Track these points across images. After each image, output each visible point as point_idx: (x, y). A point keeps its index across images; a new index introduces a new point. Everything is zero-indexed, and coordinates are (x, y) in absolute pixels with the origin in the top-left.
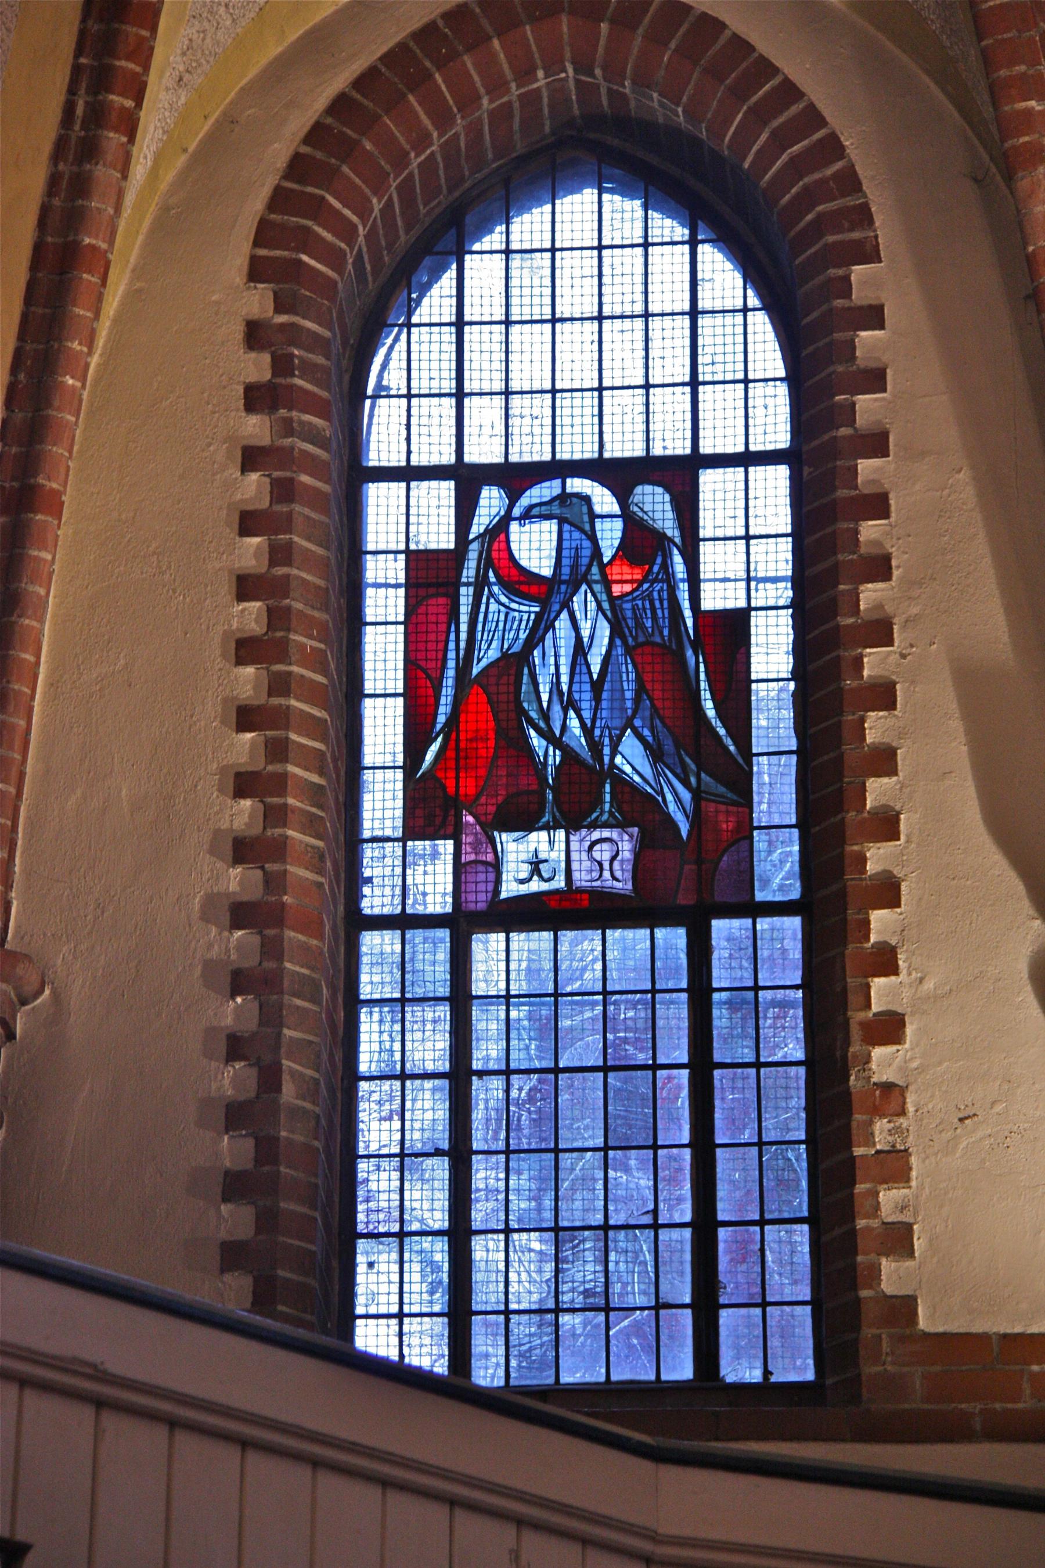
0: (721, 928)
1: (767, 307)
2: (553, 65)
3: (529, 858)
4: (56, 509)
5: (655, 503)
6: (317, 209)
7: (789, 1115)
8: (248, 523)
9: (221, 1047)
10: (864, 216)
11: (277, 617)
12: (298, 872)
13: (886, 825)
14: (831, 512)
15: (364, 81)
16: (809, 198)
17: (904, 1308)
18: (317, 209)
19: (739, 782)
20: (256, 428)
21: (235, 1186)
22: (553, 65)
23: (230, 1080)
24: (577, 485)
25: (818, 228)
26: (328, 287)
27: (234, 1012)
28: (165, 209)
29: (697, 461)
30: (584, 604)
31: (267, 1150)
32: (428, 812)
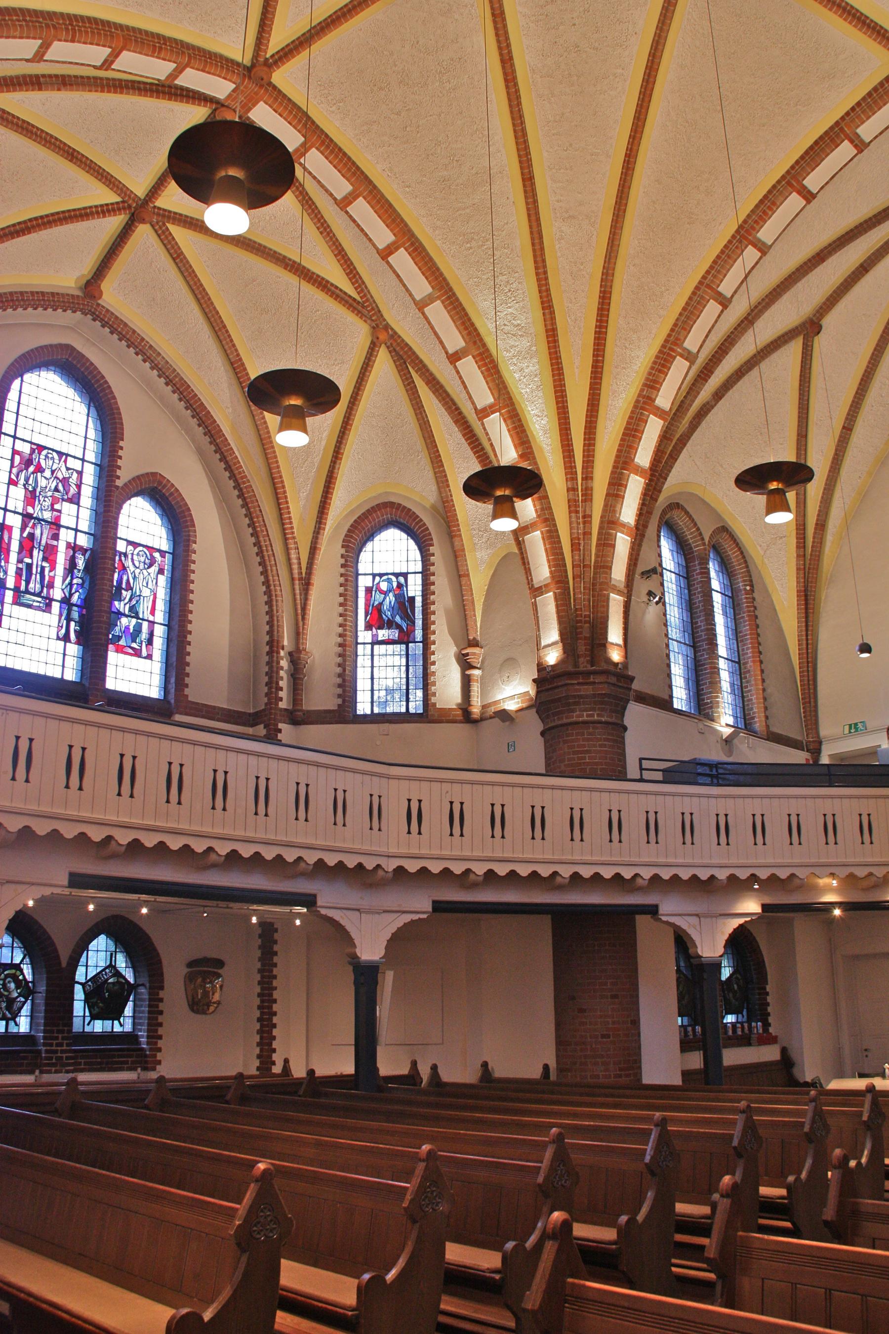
0: (410, 645)
2: (387, 514)
3: (383, 634)
4: (313, 585)
5: (402, 580)
6: (352, 537)
7: (420, 670)
8: (341, 585)
10: (432, 539)
11: (345, 600)
12: (348, 639)
13: (434, 643)
14: (426, 595)
16: (424, 536)
17: (435, 704)
18: (352, 537)
19: (414, 623)
21: (340, 686)
22: (387, 514)
24: (390, 576)
25: (425, 541)
26: (353, 549)
27: (339, 660)
29: (408, 573)
30: (391, 595)
31: (344, 680)
32: (368, 627)
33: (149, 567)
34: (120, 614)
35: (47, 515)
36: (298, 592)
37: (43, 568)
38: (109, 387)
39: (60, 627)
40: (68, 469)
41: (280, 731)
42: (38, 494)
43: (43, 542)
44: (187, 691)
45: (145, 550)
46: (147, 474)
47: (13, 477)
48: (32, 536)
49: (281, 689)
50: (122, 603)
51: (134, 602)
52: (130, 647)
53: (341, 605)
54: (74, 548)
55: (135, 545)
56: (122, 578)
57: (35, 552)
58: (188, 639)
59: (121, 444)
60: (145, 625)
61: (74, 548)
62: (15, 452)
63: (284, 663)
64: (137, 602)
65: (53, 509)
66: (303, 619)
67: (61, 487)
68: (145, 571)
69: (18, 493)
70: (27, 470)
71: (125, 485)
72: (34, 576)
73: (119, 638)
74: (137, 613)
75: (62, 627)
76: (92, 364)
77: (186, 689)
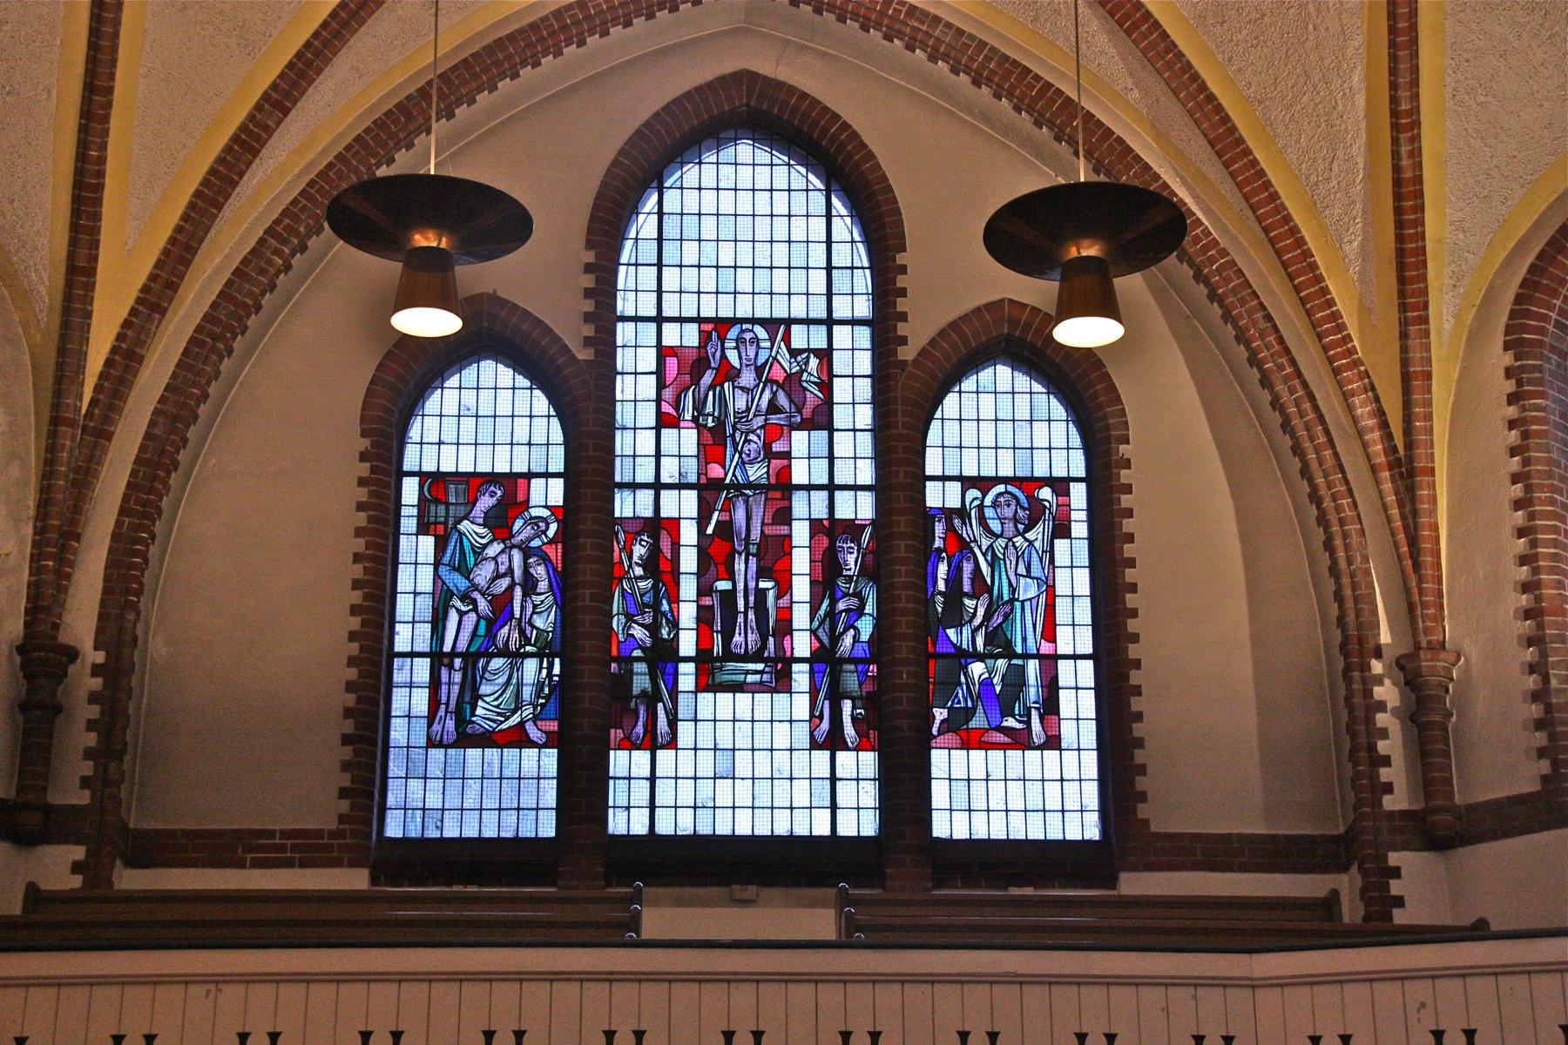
1: (559, 415)
8: (1513, 452)
9: (1527, 669)
11: (1528, 489)
15: (1540, 257)
17: (1146, 822)
18: (1527, 314)
20: (1512, 412)
21: (1539, 725)
23: (1532, 682)
27: (1530, 654)
28: (1471, 331)
33: (1028, 528)
34: (964, 657)
35: (756, 473)
36: (1391, 499)
37: (760, 594)
38: (855, 135)
39: (815, 717)
40: (794, 353)
41: (1396, 873)
42: (729, 430)
43: (756, 535)
44: (1143, 811)
45: (1010, 488)
46: (977, 310)
47: (666, 408)
48: (726, 528)
49: (1386, 761)
50: (966, 631)
51: (997, 620)
52: (999, 729)
53: (1518, 504)
54: (830, 531)
55: (983, 483)
56: (960, 569)
57: (739, 565)
58: (1133, 681)
59: (901, 259)
60: (1032, 667)
61: (830, 531)
62: (663, 352)
63: (1386, 692)
64: (1006, 616)
65: (769, 454)
66: (1417, 566)
67: (783, 400)
68: (1019, 540)
69: (687, 440)
70: (698, 384)
71: (923, 353)
72: (741, 619)
73: (969, 713)
74: (1009, 645)
75: (821, 717)
76: (804, 95)
77: (1140, 806)
